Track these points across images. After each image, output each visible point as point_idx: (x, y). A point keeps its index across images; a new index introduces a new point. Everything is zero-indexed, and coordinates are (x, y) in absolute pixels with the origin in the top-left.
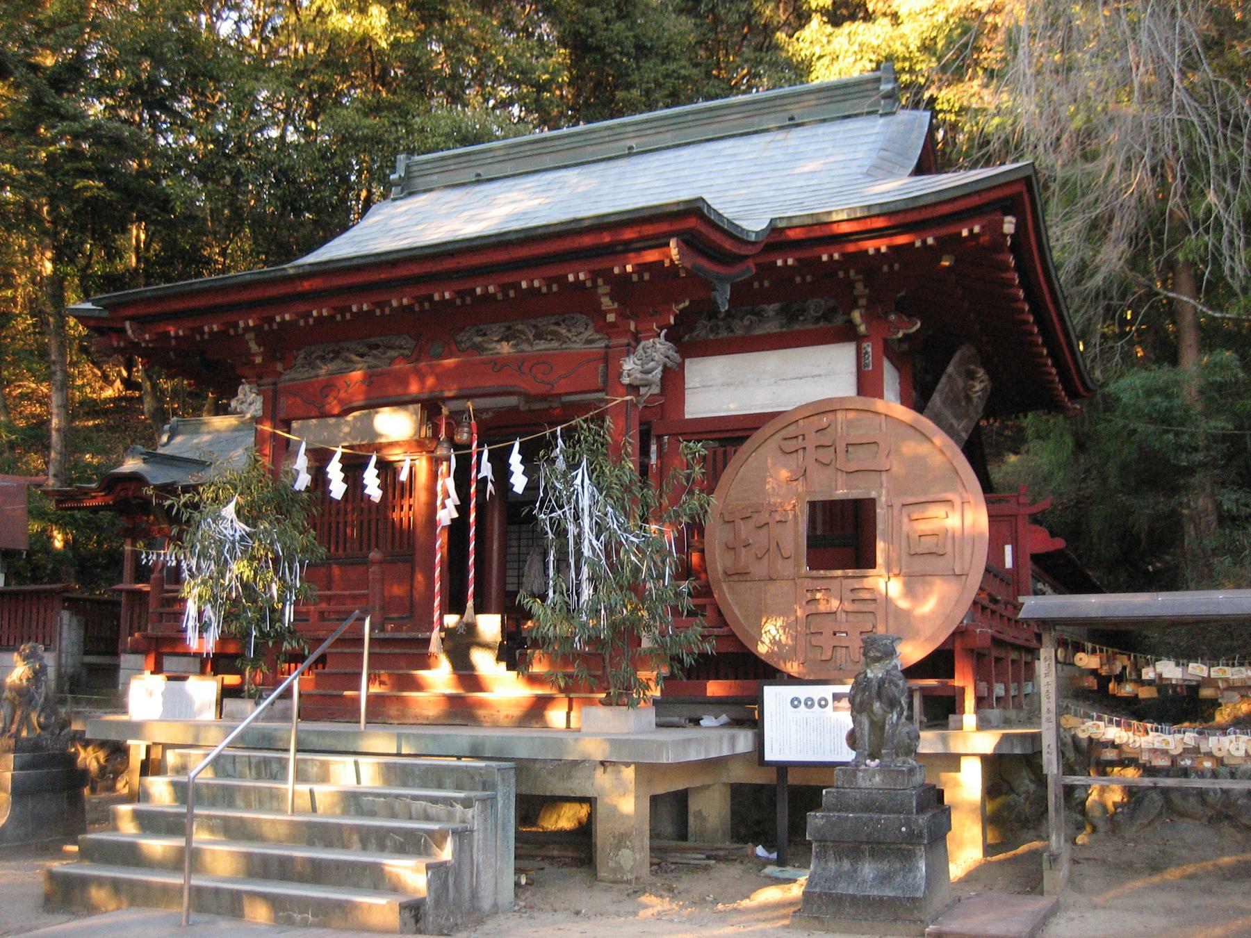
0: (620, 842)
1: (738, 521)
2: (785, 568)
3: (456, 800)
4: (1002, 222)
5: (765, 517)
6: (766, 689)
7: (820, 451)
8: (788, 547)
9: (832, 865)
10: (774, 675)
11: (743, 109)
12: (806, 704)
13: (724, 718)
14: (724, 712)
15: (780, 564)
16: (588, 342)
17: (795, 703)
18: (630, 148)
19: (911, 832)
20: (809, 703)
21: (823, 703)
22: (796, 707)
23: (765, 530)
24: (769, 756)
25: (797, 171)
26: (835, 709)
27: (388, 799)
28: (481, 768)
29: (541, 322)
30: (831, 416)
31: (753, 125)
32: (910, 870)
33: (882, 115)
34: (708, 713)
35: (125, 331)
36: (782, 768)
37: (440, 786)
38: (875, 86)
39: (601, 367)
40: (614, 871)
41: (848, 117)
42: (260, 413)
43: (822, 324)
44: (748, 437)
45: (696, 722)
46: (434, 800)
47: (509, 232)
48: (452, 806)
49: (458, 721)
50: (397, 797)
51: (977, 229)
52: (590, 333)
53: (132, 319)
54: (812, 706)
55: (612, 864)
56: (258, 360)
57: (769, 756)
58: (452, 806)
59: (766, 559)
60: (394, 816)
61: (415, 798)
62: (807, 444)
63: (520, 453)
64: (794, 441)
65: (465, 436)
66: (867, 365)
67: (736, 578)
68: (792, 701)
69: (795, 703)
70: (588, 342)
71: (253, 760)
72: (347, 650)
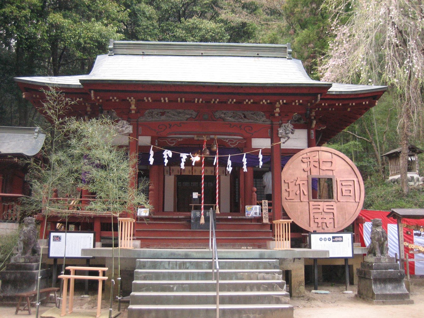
0: (300, 284)
3: (276, 272)
4: (376, 102)
7: (315, 162)
9: (378, 286)
11: (243, 48)
16: (263, 121)
17: (321, 239)
18: (202, 53)
19: (401, 275)
20: (325, 239)
21: (325, 239)
22: (321, 241)
24: (52, 255)
26: (333, 241)
27: (249, 274)
28: (274, 262)
29: (246, 113)
31: (245, 54)
32: (401, 286)
33: (288, 59)
35: (161, 101)
36: (55, 259)
37: (258, 268)
38: (285, 49)
39: (269, 130)
40: (298, 293)
41: (268, 57)
42: (131, 132)
43: (297, 123)
44: (292, 156)
46: (267, 273)
47: (268, 84)
48: (274, 274)
49: (201, 247)
50: (253, 272)
51: (367, 103)
52: (264, 119)
53: (95, 90)
55: (297, 291)
56: (133, 112)
58: (274, 274)
60: (251, 279)
61: (260, 273)
62: (311, 160)
63: (152, 150)
65: (215, 148)
66: (312, 137)
69: (321, 239)
70: (263, 121)
71: (178, 263)
72: (236, 223)
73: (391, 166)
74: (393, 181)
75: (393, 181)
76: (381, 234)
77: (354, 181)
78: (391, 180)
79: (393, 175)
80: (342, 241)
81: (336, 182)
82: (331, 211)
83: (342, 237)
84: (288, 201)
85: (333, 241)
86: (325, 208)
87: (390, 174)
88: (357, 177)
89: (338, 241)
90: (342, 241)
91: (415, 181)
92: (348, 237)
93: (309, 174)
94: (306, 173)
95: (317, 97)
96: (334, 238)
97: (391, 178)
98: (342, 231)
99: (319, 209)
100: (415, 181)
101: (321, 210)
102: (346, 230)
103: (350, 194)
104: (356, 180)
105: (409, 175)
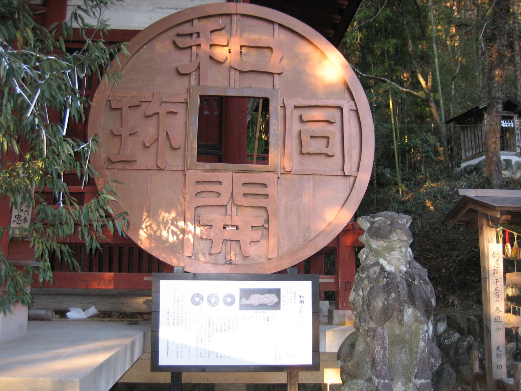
1: (125, 109)
2: (175, 161)
5: (153, 108)
6: (162, 282)
8: (178, 140)
10: (164, 270)
12: (209, 301)
13: (93, 310)
14: (92, 304)
15: (169, 154)
22: (197, 304)
23: (154, 119)
25: (60, 257)
30: (227, 19)
34: (75, 305)
36: (176, 372)
45: (62, 314)
54: (232, 303)
57: (163, 360)
59: (153, 149)
64: (188, 39)
67: (120, 166)
68: (193, 298)
73: (466, 139)
74: (469, 168)
75: (468, 170)
76: (403, 289)
77: (341, 109)
78: (465, 168)
79: (468, 159)
80: (277, 306)
81: (281, 111)
82: (262, 202)
83: (277, 292)
84: (115, 166)
85: (243, 307)
86: (240, 190)
87: (464, 158)
88: (353, 99)
89: (263, 306)
90: (277, 306)
91: (515, 169)
92: (299, 293)
93: (193, 83)
94: (186, 79)
95: (474, 262)
96: (246, 293)
97: (463, 165)
98: (283, 275)
99: (219, 194)
100: (515, 169)
101: (224, 199)
102: (304, 269)
103: (325, 150)
104: (347, 105)
105: (504, 156)
